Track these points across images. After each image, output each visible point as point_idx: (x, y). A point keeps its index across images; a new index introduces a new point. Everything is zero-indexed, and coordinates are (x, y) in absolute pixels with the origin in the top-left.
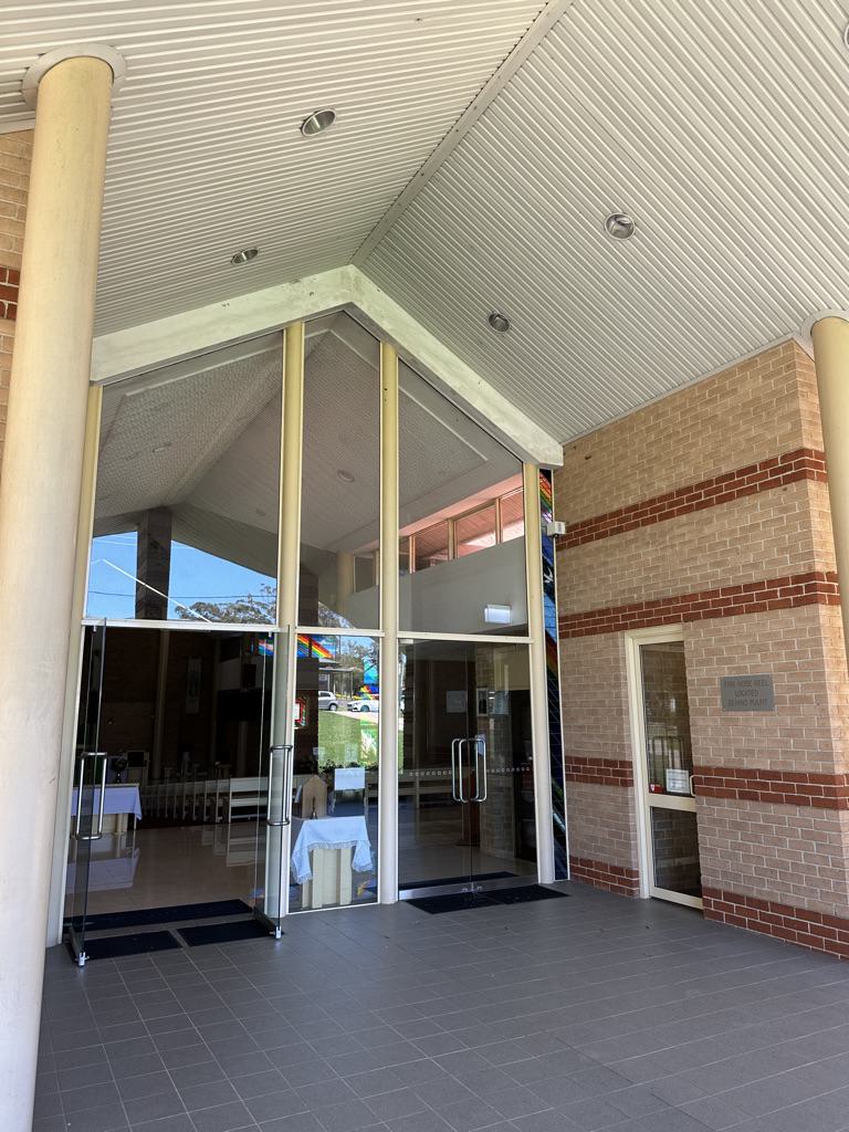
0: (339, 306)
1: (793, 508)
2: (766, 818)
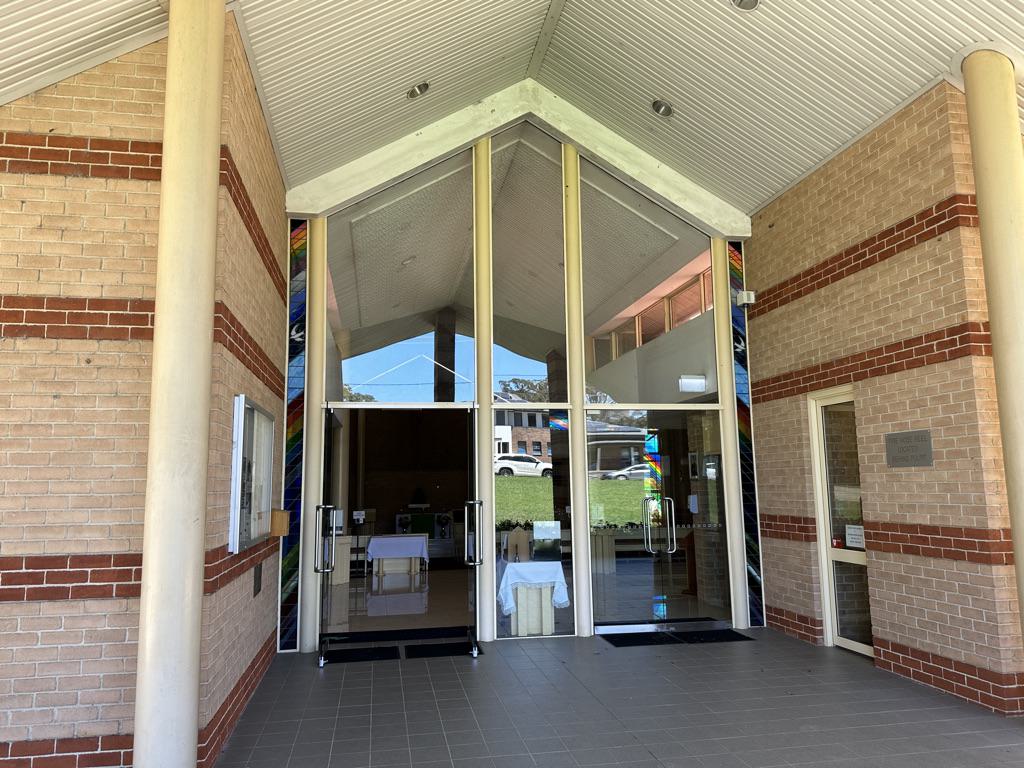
0: (520, 118)
1: (947, 258)
2: (927, 572)
